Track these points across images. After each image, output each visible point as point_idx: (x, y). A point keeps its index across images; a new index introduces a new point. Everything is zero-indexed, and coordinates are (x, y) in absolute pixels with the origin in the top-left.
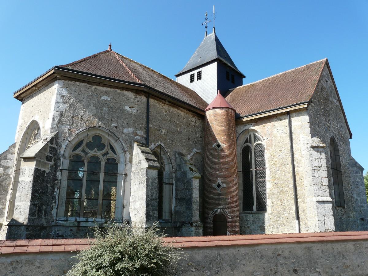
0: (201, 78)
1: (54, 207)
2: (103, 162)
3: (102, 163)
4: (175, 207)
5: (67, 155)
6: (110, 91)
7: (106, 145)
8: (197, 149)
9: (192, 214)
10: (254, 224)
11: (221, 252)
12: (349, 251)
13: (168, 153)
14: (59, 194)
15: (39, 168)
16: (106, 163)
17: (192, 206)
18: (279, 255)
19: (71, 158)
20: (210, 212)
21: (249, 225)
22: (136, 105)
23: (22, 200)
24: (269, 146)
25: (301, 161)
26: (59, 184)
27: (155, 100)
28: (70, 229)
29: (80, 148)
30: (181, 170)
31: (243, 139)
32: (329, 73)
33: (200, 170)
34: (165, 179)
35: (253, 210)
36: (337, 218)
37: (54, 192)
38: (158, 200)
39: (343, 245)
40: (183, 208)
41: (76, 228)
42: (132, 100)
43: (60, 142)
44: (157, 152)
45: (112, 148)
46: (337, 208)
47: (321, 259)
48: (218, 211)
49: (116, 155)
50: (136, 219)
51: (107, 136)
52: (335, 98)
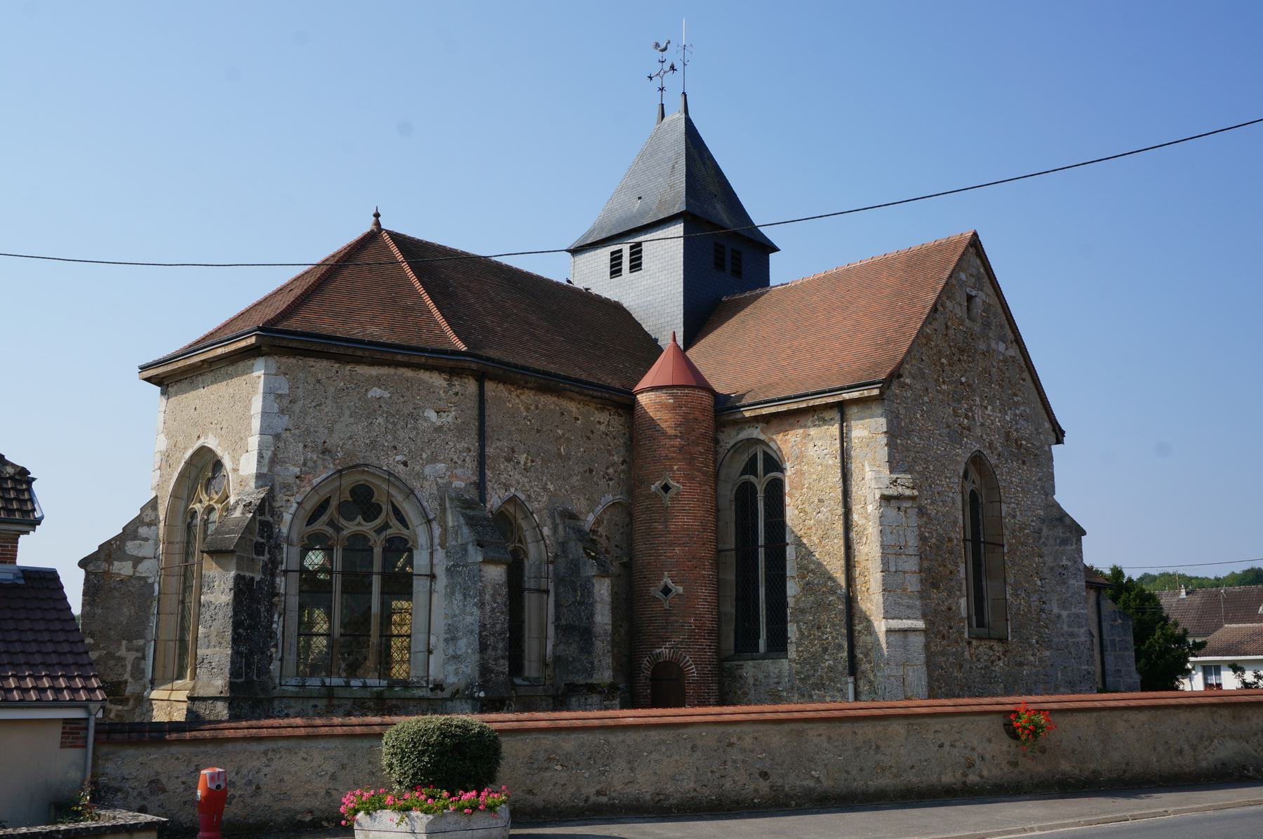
0: (640, 265)
1: (274, 656)
2: (378, 549)
3: (375, 550)
4: (554, 645)
5: (295, 537)
6: (388, 376)
7: (384, 507)
8: (613, 496)
9: (592, 663)
10: (757, 685)
11: (612, 739)
12: (894, 738)
13: (535, 515)
14: (284, 627)
15: (242, 574)
16: (385, 550)
17: (593, 644)
18: (731, 745)
19: (304, 541)
20: (646, 657)
21: (745, 689)
22: (451, 405)
23: (213, 643)
24: (797, 489)
25: (864, 529)
26: (283, 603)
27: (499, 382)
28: (313, 702)
29: (324, 518)
30: (567, 557)
31: (733, 472)
32: (982, 270)
33: (622, 549)
34: (529, 578)
35: (758, 652)
36: (971, 668)
37: (272, 623)
38: (508, 635)
39: (879, 726)
40: (571, 650)
41: (324, 702)
42: (441, 392)
43: (278, 508)
44: (507, 514)
45: (398, 513)
46: (974, 643)
47: (823, 753)
48: (663, 654)
49: (408, 529)
50: (459, 679)
51: (385, 486)
52: (1002, 338)
